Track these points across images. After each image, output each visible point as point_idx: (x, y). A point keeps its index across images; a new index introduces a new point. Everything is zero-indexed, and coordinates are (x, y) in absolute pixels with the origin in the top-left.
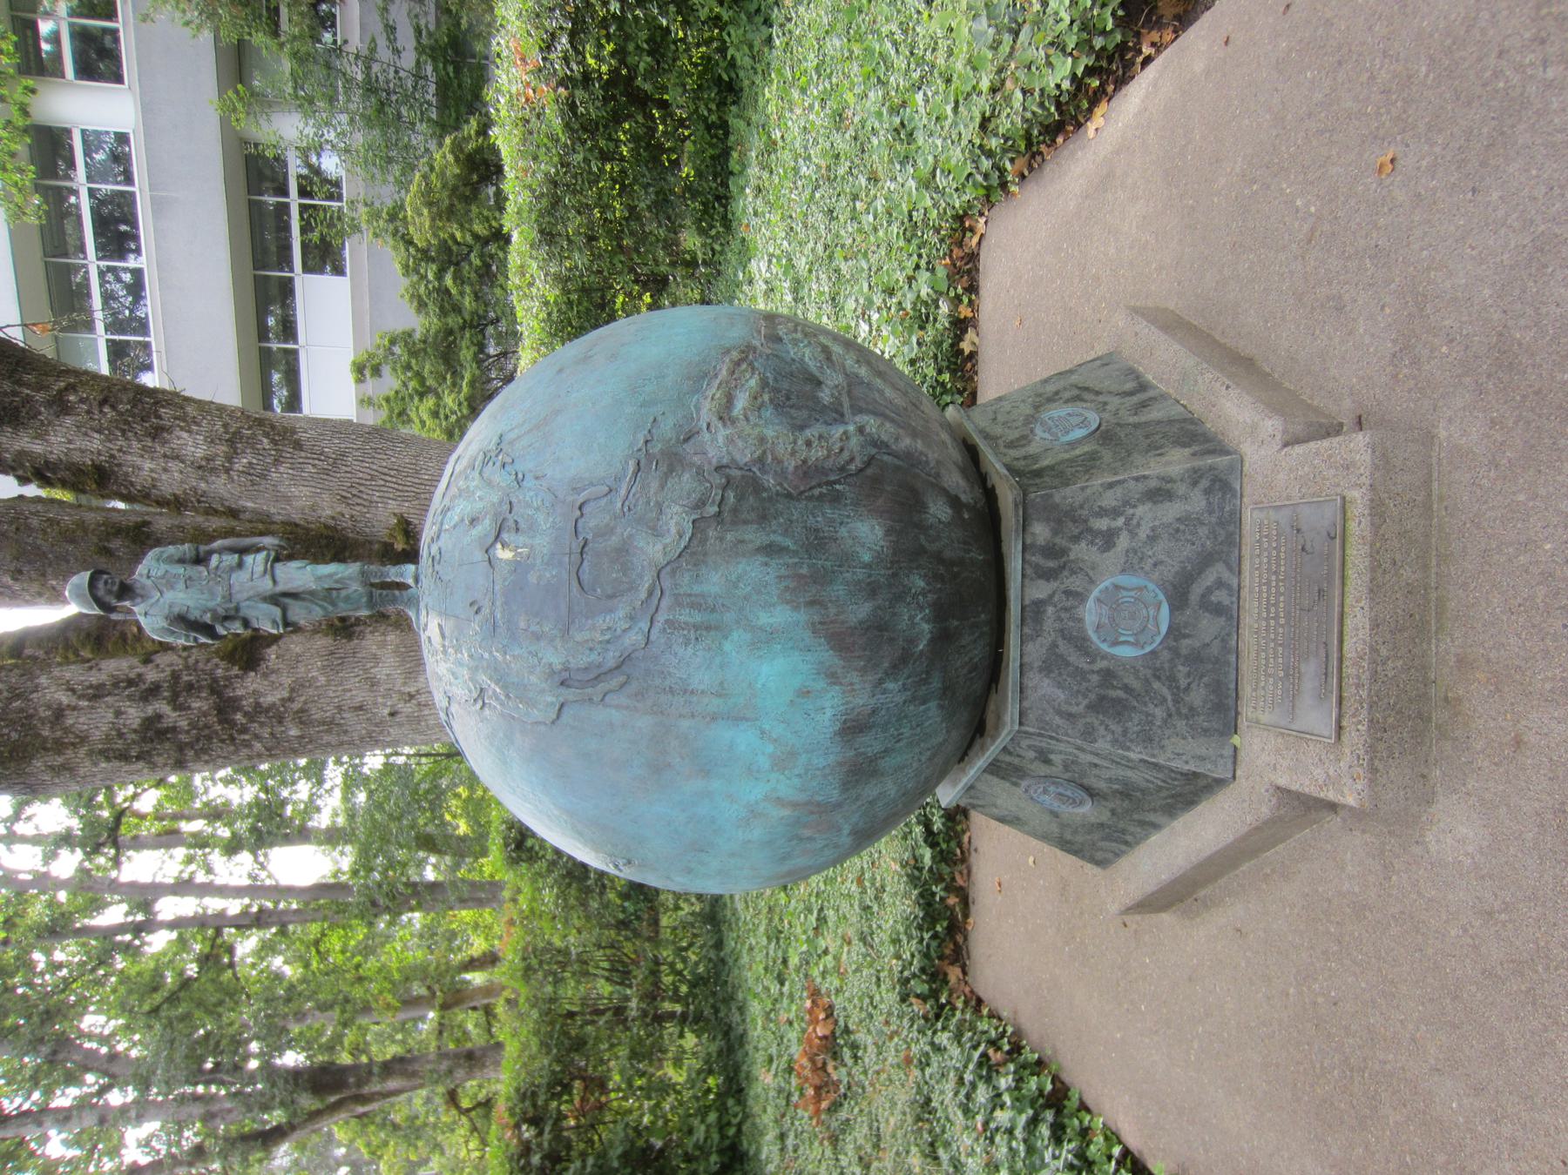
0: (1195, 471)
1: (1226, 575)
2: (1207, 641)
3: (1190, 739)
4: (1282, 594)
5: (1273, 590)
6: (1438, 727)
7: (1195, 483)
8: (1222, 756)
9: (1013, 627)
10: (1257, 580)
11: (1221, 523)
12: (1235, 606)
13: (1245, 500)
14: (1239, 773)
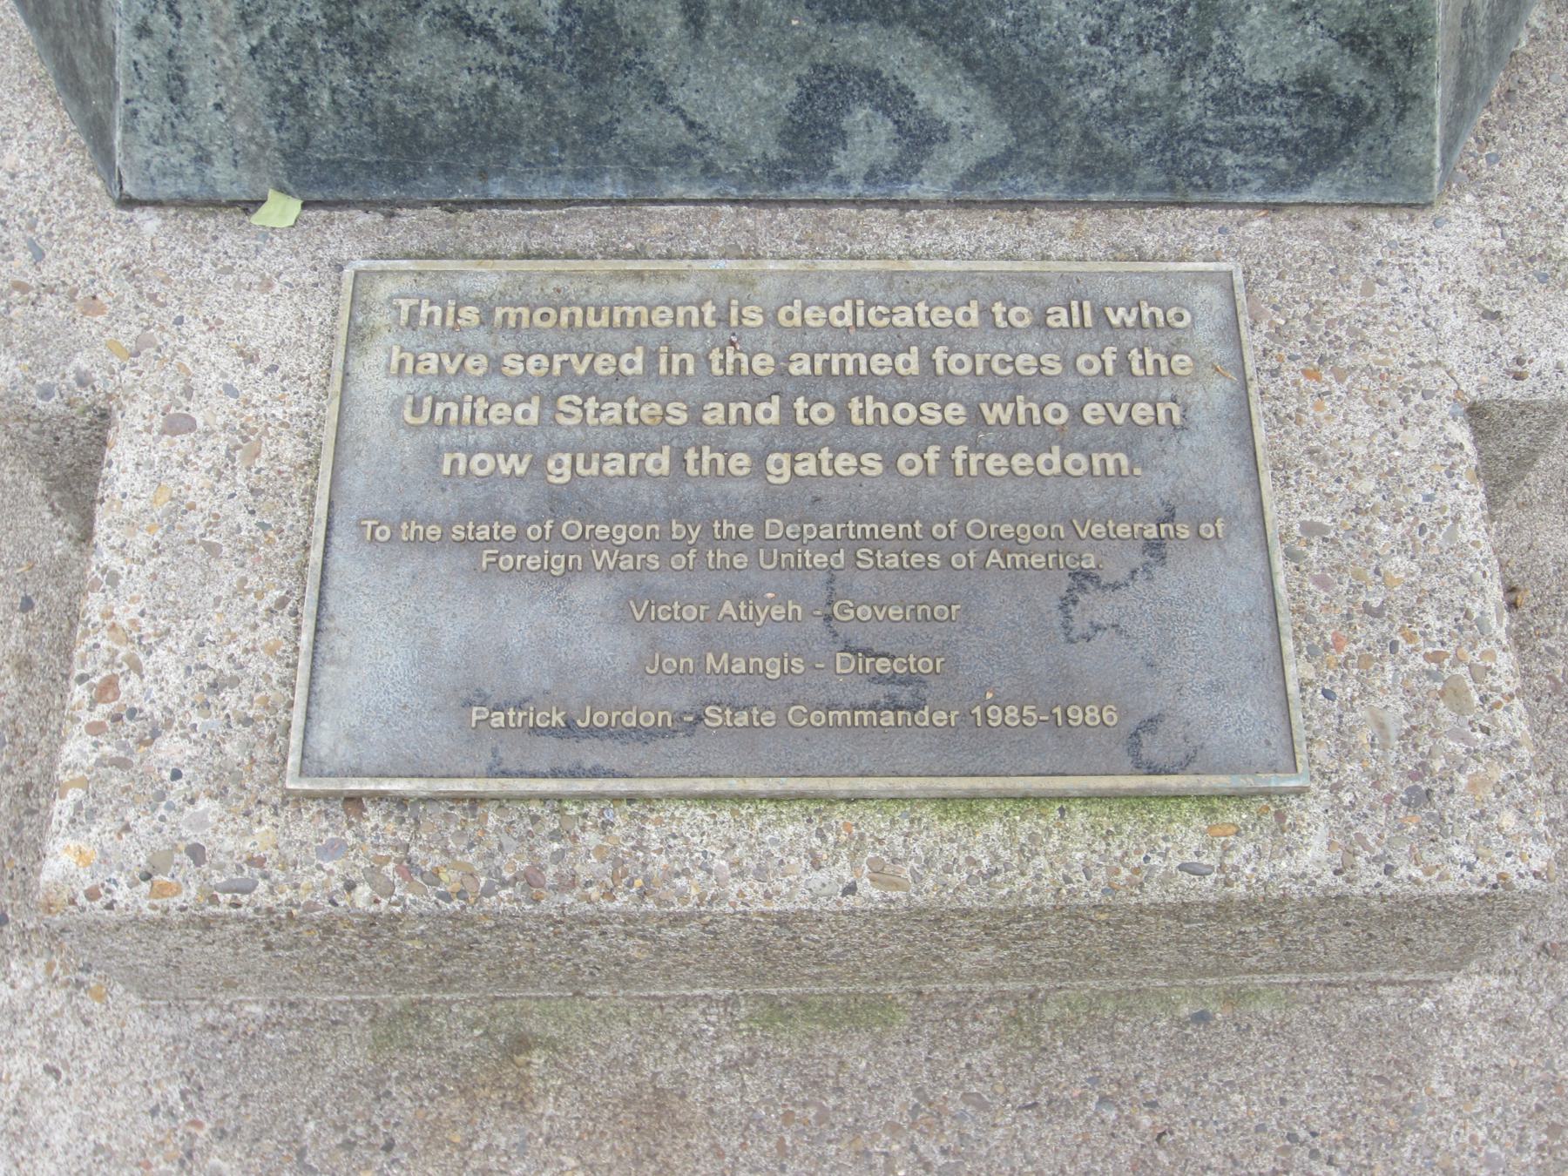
0: (1412, 43)
1: (958, 158)
2: (679, 96)
3: (245, 42)
4: (890, 464)
5: (905, 415)
6: (418, 1014)
7: (1355, 41)
8: (203, 159)
9: (1052, 786)
10: (941, 317)
11: (1172, 134)
12: (828, 191)
13: (1259, 223)
14: (149, 222)
